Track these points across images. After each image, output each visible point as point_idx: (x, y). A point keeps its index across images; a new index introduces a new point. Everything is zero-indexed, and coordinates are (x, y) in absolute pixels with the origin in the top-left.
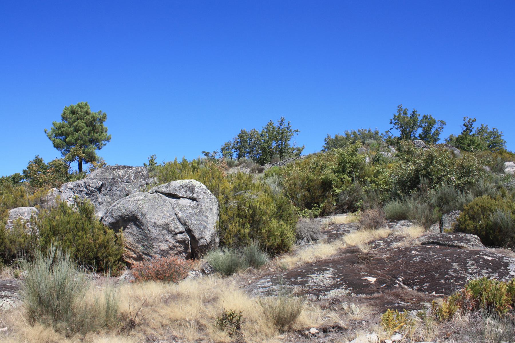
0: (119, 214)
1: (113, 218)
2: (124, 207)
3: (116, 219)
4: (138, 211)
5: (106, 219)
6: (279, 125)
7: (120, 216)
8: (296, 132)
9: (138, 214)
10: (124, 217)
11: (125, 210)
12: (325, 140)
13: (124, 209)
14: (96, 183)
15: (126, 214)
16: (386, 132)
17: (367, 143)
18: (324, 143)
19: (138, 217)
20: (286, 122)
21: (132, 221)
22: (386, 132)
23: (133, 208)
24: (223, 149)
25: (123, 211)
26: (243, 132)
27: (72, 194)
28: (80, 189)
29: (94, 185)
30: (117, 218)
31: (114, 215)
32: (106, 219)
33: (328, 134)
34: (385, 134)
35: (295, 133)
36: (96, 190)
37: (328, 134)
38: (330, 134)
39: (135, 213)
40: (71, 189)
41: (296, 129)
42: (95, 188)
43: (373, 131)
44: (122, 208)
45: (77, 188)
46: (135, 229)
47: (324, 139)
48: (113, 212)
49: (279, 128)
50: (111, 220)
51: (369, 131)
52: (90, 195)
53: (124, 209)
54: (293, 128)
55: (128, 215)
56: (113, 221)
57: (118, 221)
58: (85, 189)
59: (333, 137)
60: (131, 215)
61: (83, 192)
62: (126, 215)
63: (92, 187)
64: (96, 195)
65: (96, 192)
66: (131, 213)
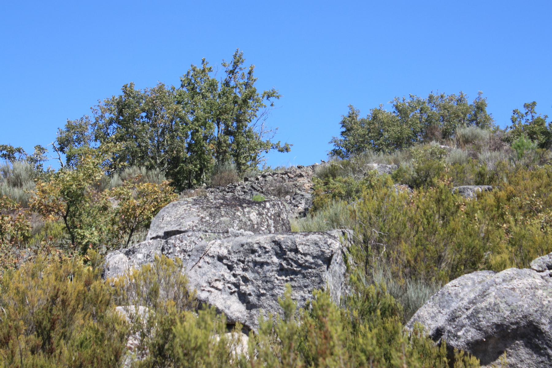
0: (495, 320)
1: (480, 329)
2: (506, 303)
3: (486, 332)
4: (542, 314)
5: (459, 334)
6: (225, 76)
7: (498, 326)
8: (268, 97)
9: (543, 321)
10: (508, 327)
11: (512, 312)
12: (343, 124)
13: (509, 308)
14: (321, 243)
15: (513, 320)
16: (526, 106)
17: (463, 136)
18: (337, 131)
19: (542, 327)
20: (245, 67)
21: (522, 337)
22: (526, 106)
23: (529, 306)
24: (63, 145)
25: (508, 313)
26: (127, 91)
27: (224, 271)
28: (258, 259)
29: (314, 250)
30: (490, 330)
31: (484, 323)
32: (459, 334)
33: (351, 107)
34: (523, 111)
35: (265, 102)
36: (320, 262)
37: (351, 107)
38: (356, 107)
39: (536, 317)
40: (220, 259)
41: (268, 90)
42: (314, 257)
43: (470, 101)
44: (502, 306)
45: (246, 255)
46: (527, 356)
47: (341, 119)
48: (480, 315)
49: (227, 84)
50: (472, 334)
51: (460, 100)
52: (295, 273)
53: (509, 308)
54: (260, 88)
55: (517, 323)
56: (478, 336)
57: (489, 337)
58: (275, 260)
59: (364, 114)
60: (523, 323)
61: (266, 268)
62: (512, 324)
63: (305, 255)
64: (318, 276)
65: (320, 265)
66: (525, 317)
